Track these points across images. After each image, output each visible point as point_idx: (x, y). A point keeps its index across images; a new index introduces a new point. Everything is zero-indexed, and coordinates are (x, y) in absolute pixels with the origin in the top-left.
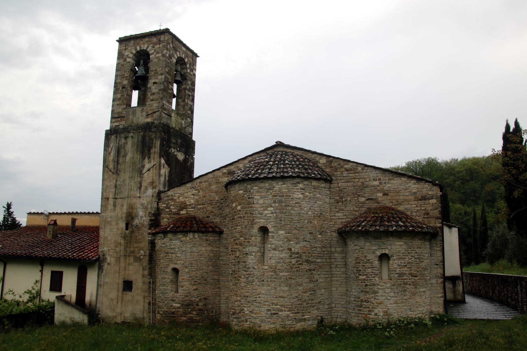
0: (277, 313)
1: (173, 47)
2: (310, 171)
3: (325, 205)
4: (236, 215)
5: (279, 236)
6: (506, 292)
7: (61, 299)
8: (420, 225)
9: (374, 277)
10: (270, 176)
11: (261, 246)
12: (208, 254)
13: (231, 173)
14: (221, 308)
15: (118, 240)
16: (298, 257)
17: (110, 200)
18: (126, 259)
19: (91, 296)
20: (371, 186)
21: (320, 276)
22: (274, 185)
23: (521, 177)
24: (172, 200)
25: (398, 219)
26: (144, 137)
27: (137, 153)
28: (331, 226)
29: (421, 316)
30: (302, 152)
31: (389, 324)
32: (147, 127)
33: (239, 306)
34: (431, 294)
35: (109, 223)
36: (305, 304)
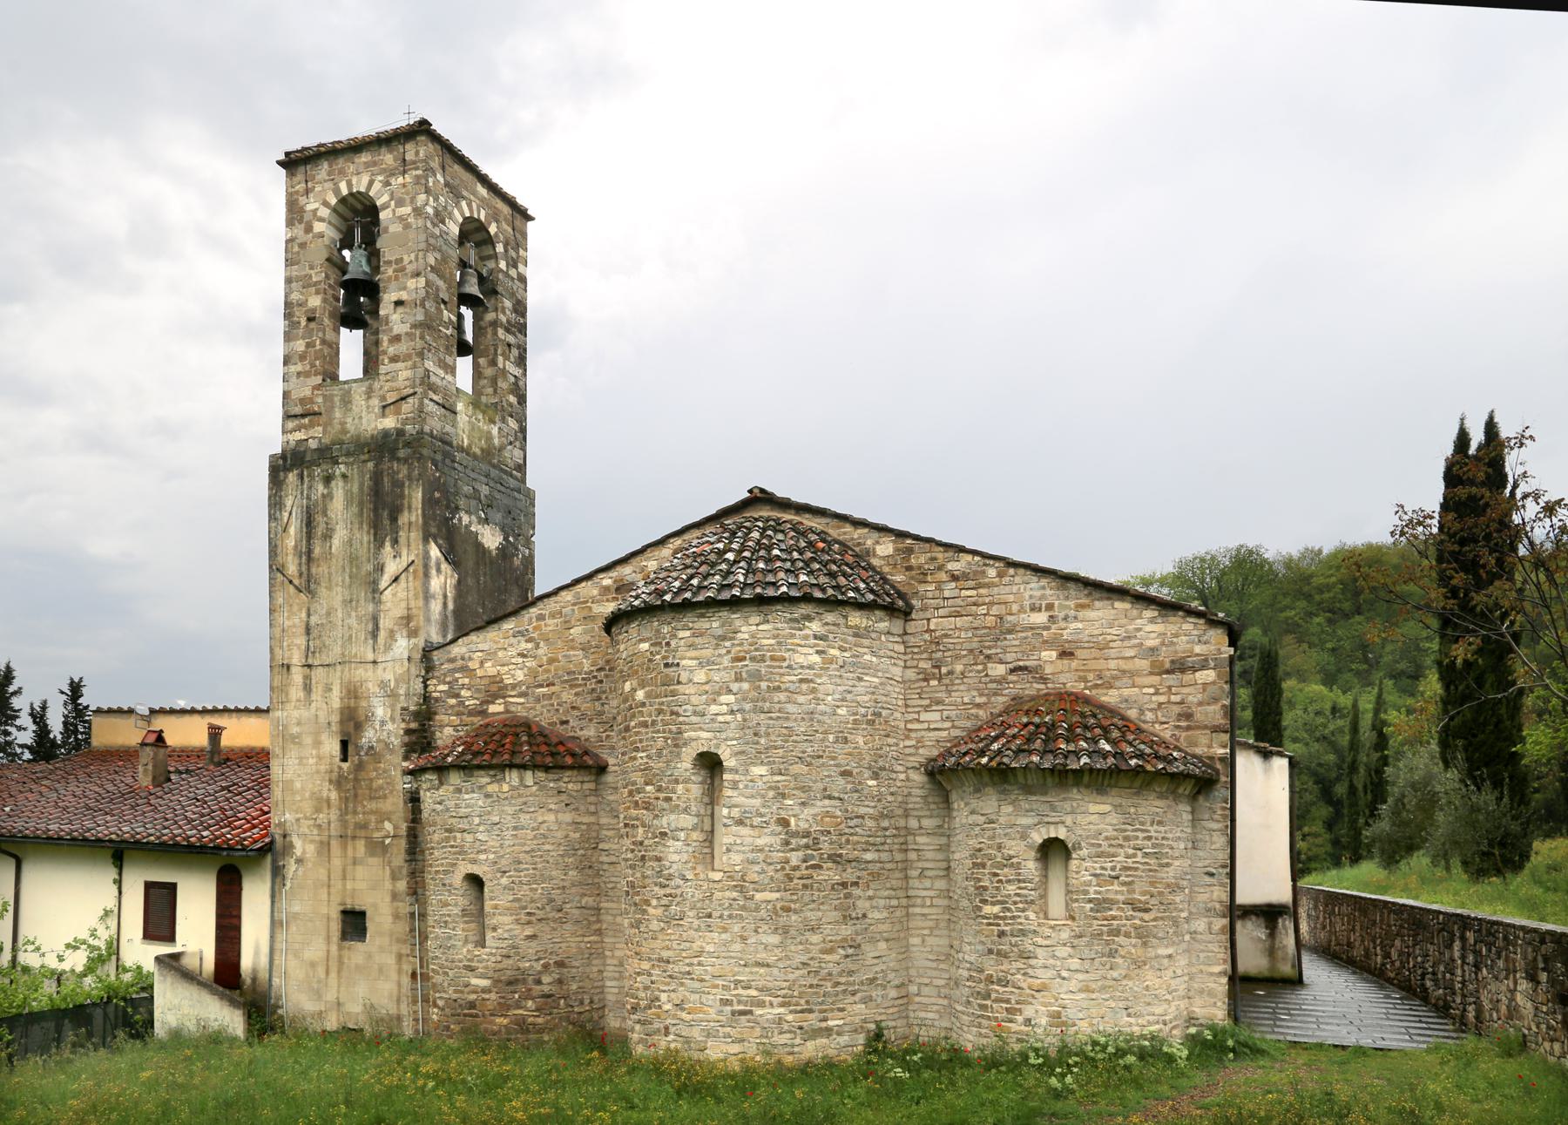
0: (750, 1012)
1: (447, 184)
2: (842, 581)
3: (889, 688)
4: (633, 716)
5: (752, 781)
6: (1419, 959)
7: (171, 963)
8: (1162, 752)
9: (1023, 910)
10: (725, 595)
11: (702, 812)
12: (565, 833)
13: (622, 588)
14: (606, 990)
15: (320, 791)
16: (807, 847)
17: (294, 670)
18: (344, 847)
19: (257, 953)
20: (1025, 629)
21: (874, 903)
22: (738, 623)
23: (1479, 599)
24: (464, 669)
25: (1098, 731)
26: (377, 477)
27: (361, 528)
28: (908, 751)
29: (1161, 1030)
30: (824, 520)
31: (1064, 1051)
32: (383, 447)
33: (646, 988)
34: (1190, 964)
35: (295, 739)
36: (829, 984)
